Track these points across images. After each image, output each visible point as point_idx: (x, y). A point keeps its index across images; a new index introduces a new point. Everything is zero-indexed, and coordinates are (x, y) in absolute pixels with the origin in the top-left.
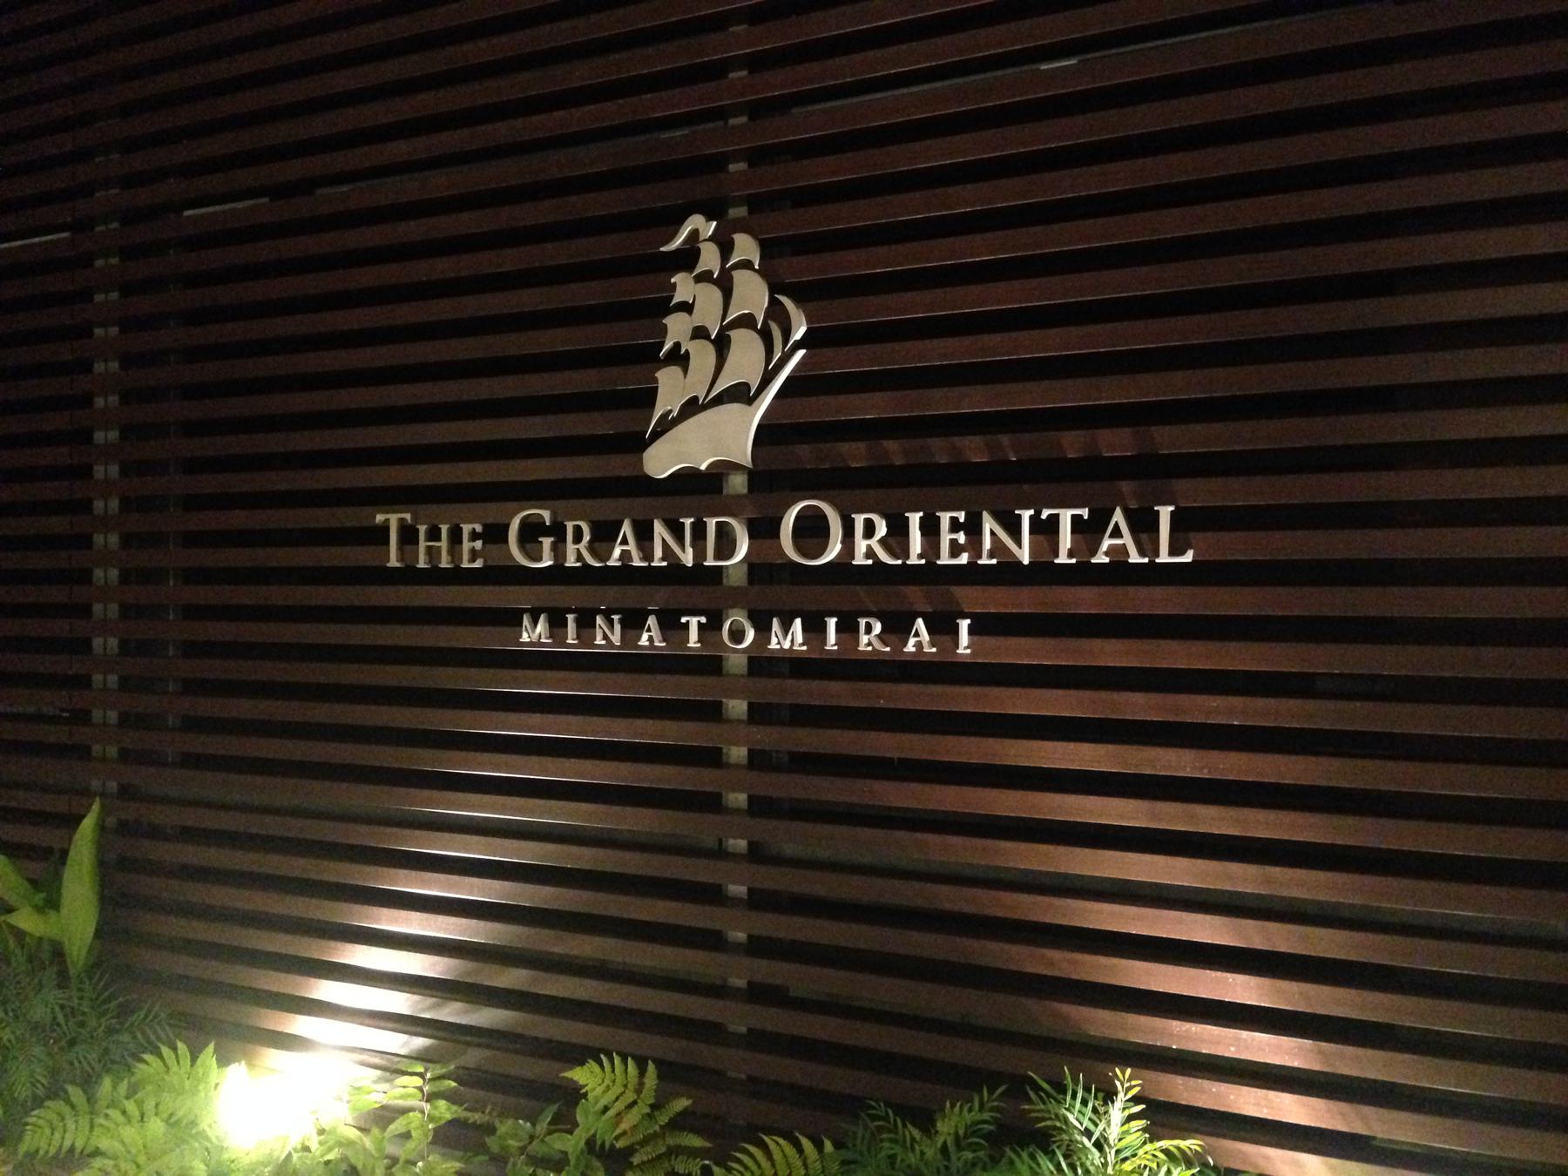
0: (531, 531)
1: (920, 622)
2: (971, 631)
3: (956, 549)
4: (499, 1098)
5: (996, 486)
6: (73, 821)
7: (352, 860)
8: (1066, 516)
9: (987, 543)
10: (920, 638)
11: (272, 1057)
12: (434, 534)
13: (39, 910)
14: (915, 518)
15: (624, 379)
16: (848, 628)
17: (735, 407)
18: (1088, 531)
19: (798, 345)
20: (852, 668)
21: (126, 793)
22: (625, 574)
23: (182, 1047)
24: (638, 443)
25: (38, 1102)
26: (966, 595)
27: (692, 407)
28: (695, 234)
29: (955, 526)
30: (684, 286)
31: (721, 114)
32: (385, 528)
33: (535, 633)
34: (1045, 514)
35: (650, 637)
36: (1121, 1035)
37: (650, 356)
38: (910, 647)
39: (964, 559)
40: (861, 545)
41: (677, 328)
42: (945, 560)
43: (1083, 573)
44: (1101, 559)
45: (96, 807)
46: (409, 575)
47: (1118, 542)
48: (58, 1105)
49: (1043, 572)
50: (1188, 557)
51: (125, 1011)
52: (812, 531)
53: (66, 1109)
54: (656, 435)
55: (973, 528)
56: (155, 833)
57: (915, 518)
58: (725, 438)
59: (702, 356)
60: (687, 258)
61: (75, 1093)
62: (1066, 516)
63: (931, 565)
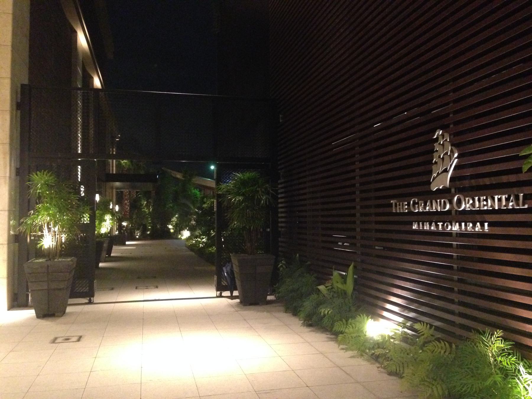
0: (415, 203)
2: (488, 226)
3: (484, 206)
5: (489, 190)
6: (349, 266)
7: (505, 304)
8: (504, 197)
9: (489, 204)
10: (478, 228)
11: (381, 320)
12: (400, 205)
13: (342, 284)
14: (477, 198)
15: (468, 161)
16: (482, 226)
17: (444, 173)
18: (507, 200)
19: (456, 158)
21: (363, 262)
22: (429, 213)
23: (365, 315)
25: (338, 321)
26: (488, 217)
28: (438, 134)
29: (484, 200)
30: (437, 147)
31: (448, 104)
32: (392, 204)
33: (415, 227)
34: (499, 197)
35: (478, 228)
36: (517, 327)
39: (486, 208)
44: (511, 207)
45: (353, 263)
46: (397, 214)
48: (341, 322)
49: (500, 211)
50: (526, 206)
51: (359, 307)
52: (459, 202)
53: (342, 323)
55: (486, 200)
56: (370, 271)
59: (440, 162)
60: (437, 139)
62: (504, 197)
63: (499, 209)
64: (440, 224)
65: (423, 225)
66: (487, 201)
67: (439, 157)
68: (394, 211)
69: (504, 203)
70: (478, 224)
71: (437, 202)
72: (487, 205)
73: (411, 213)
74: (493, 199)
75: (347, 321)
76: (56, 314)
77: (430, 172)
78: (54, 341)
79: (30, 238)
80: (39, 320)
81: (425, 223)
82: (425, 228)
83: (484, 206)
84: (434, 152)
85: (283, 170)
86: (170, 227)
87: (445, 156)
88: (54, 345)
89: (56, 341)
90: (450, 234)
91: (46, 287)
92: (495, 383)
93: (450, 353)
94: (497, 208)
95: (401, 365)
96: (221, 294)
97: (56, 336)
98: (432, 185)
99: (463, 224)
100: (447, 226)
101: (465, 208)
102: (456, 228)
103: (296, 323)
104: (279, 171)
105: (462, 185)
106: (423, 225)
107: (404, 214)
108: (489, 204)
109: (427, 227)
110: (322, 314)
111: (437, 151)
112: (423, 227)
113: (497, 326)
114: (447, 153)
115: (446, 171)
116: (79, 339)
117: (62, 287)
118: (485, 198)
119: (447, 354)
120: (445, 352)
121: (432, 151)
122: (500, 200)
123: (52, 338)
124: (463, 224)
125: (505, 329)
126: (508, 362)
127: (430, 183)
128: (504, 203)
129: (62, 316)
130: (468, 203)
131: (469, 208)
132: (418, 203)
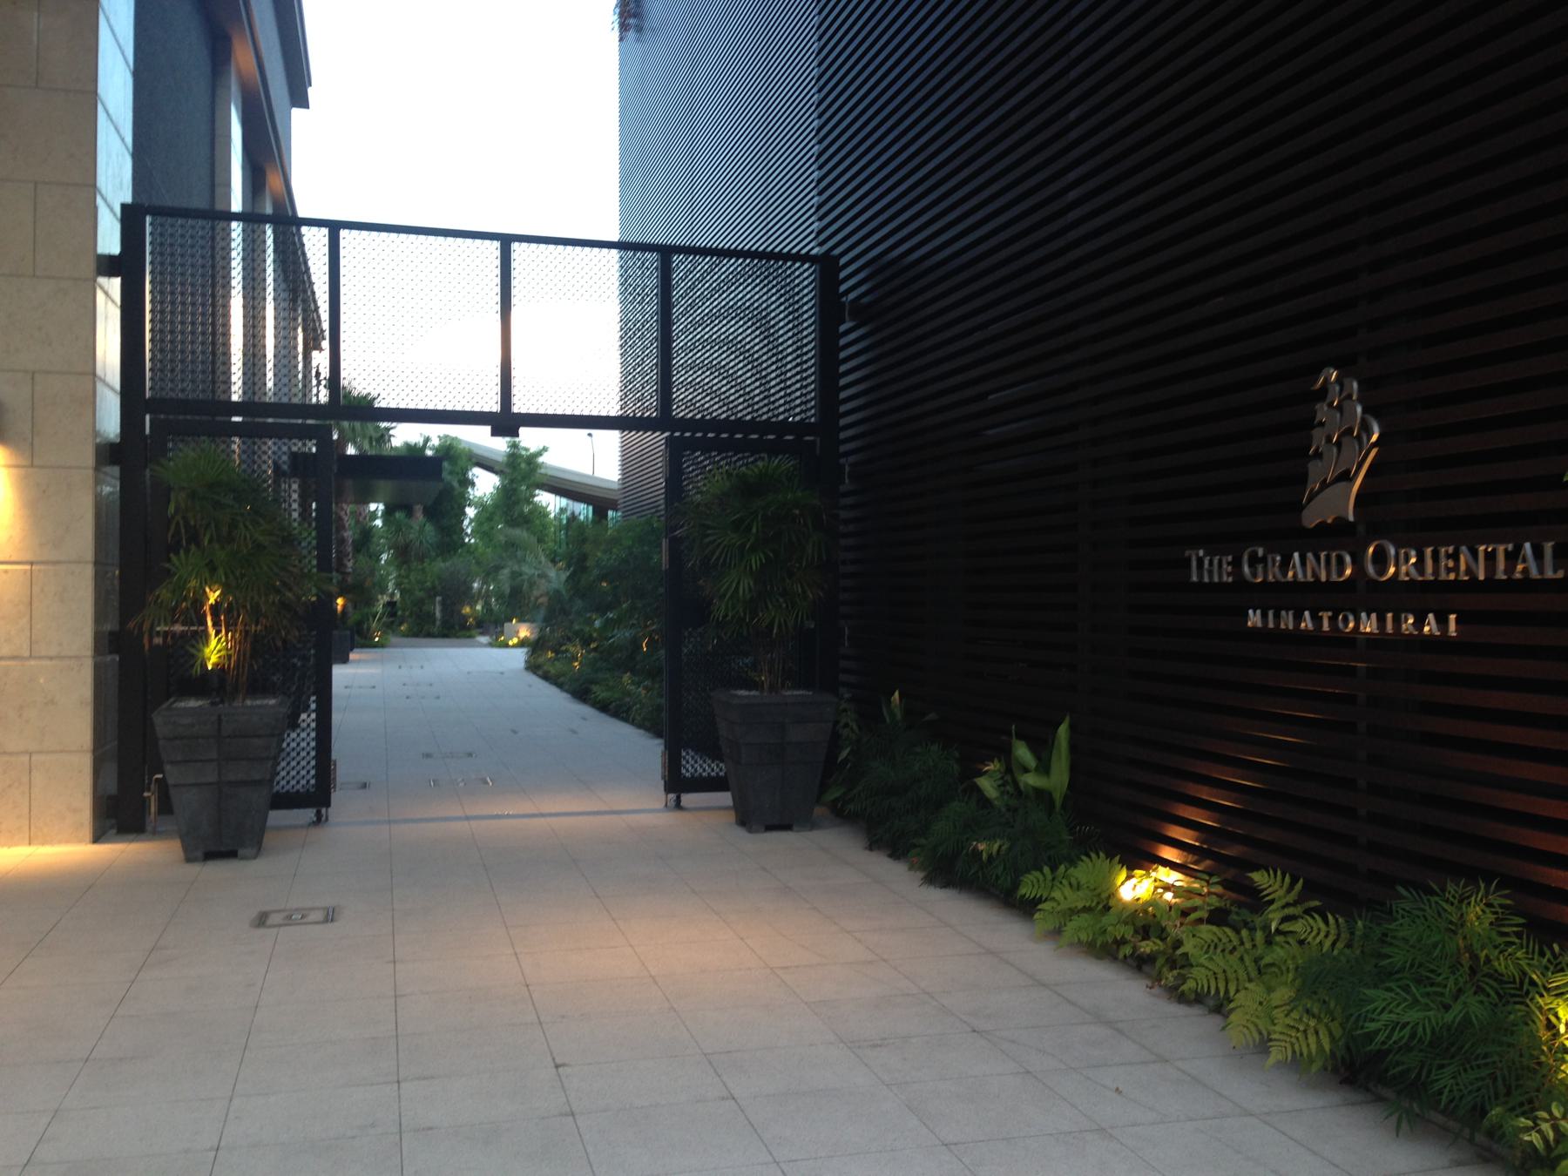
1: (1431, 616)
2: (1457, 620)
3: (1449, 570)
4: (1234, 895)
5: (1465, 530)
8: (1501, 548)
9: (1463, 567)
14: (1429, 551)
16: (1442, 621)
18: (1512, 557)
20: (1297, 637)
24: (1298, 508)
25: (1028, 871)
27: (1325, 485)
29: (1448, 556)
30: (1322, 412)
35: (1307, 623)
37: (1302, 453)
38: (1426, 629)
39: (1452, 576)
40: (1404, 569)
41: (1318, 436)
42: (1443, 576)
43: (1510, 585)
44: (1518, 576)
47: (1528, 565)
48: (1037, 874)
49: (1491, 584)
52: (1381, 559)
54: (1310, 500)
55: (1455, 556)
57: (1323, 555)
58: (1345, 502)
60: (1323, 394)
61: (1046, 870)
62: (1501, 548)
64: (1325, 616)
65: (1277, 617)
66: (1457, 560)
67: (1329, 439)
68: (1195, 579)
69: (1501, 564)
70: (1431, 616)
71: (1318, 559)
72: (1456, 569)
73: (1241, 584)
74: (1474, 553)
75: (1054, 869)
76: (241, 852)
77: (1303, 479)
78: (262, 920)
79: (151, 641)
80: (195, 869)
81: (1283, 613)
82: (1283, 626)
83: (1449, 570)
84: (1313, 427)
85: (852, 459)
86: (479, 607)
87: (1345, 440)
88: (262, 931)
89: (269, 922)
90: (1352, 641)
91: (213, 778)
92: (1466, 1021)
93: (1349, 946)
94: (1482, 577)
95: (1221, 976)
96: (678, 800)
97: (267, 908)
98: (1305, 513)
99: (1271, 613)
100: (1346, 621)
101: (1397, 573)
102: (1369, 626)
103: (899, 876)
104: (842, 461)
105: (1384, 513)
106: (1277, 617)
107: (1222, 586)
108: (1463, 567)
109: (1288, 621)
110: (985, 856)
111: (1321, 424)
112: (1277, 623)
113: (1471, 874)
114: (1350, 431)
115: (1346, 477)
116: (330, 916)
117: (257, 777)
118: (1451, 549)
119: (1340, 945)
120: (1334, 944)
121: (1310, 423)
122: (1491, 557)
123: (253, 913)
124: (1271, 613)
125: (1506, 882)
126: (1515, 960)
127: (1303, 508)
128: (1501, 564)
129: (255, 858)
130: (1407, 559)
131: (1407, 574)
132: (1264, 560)
